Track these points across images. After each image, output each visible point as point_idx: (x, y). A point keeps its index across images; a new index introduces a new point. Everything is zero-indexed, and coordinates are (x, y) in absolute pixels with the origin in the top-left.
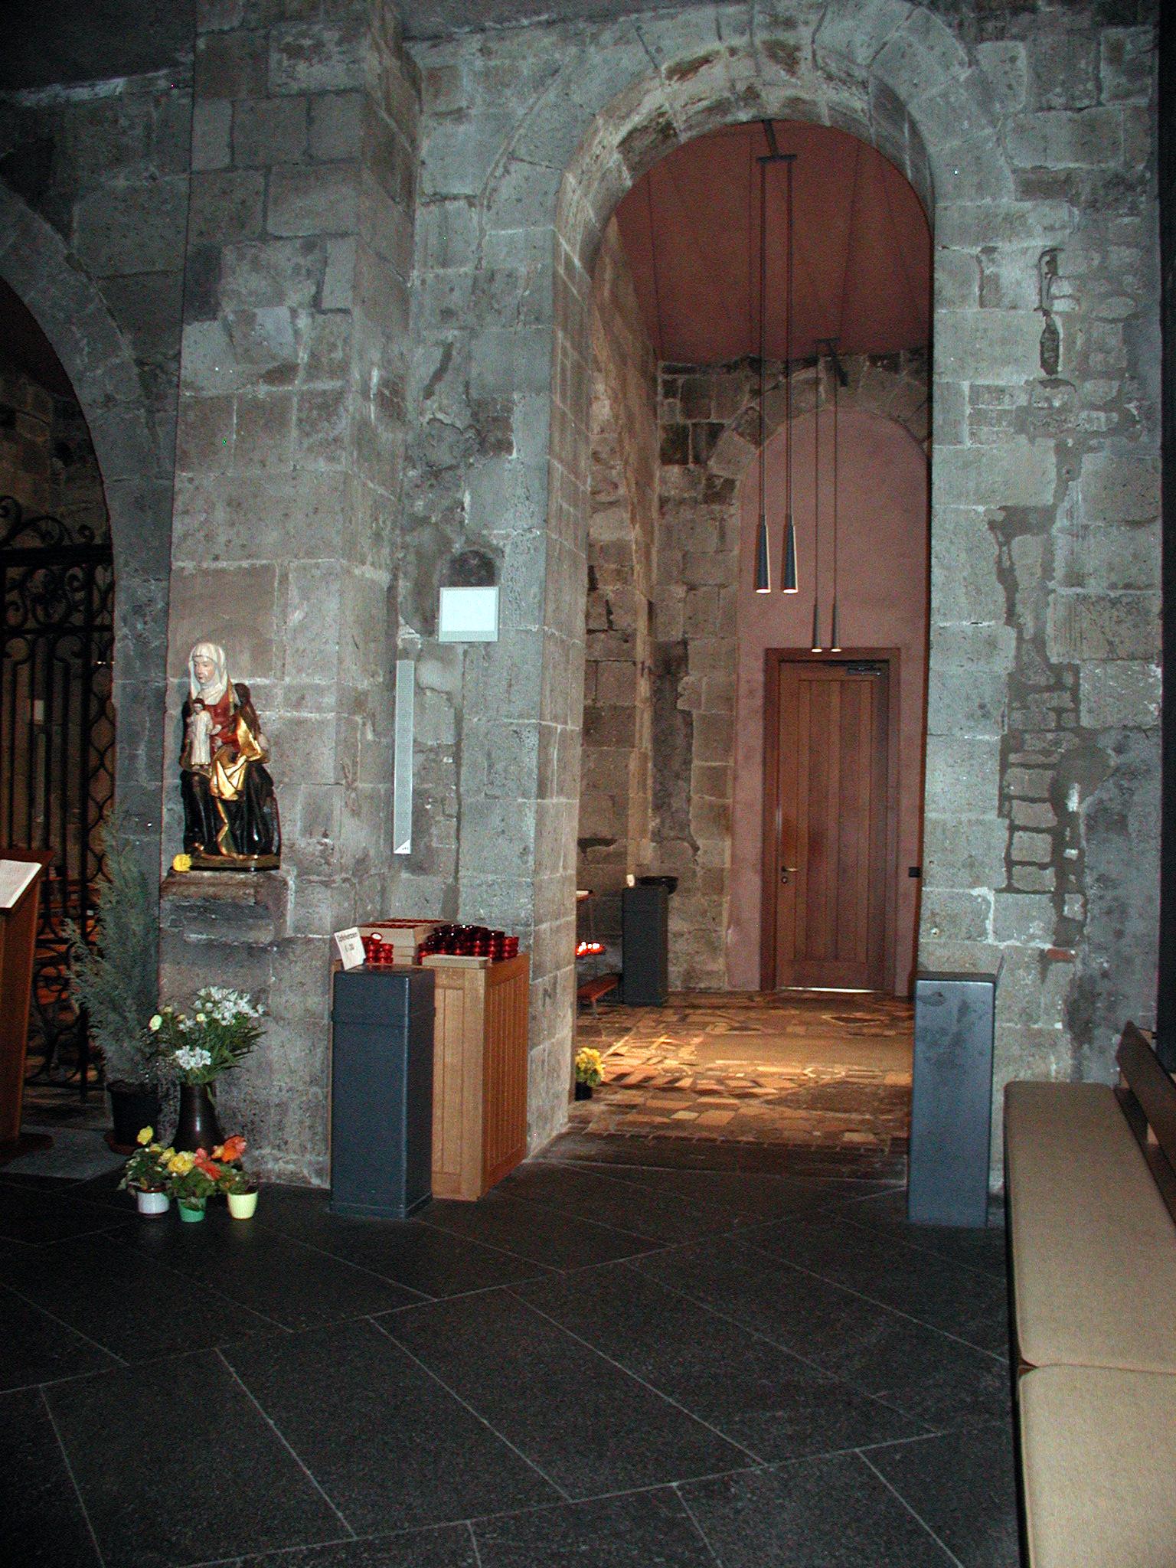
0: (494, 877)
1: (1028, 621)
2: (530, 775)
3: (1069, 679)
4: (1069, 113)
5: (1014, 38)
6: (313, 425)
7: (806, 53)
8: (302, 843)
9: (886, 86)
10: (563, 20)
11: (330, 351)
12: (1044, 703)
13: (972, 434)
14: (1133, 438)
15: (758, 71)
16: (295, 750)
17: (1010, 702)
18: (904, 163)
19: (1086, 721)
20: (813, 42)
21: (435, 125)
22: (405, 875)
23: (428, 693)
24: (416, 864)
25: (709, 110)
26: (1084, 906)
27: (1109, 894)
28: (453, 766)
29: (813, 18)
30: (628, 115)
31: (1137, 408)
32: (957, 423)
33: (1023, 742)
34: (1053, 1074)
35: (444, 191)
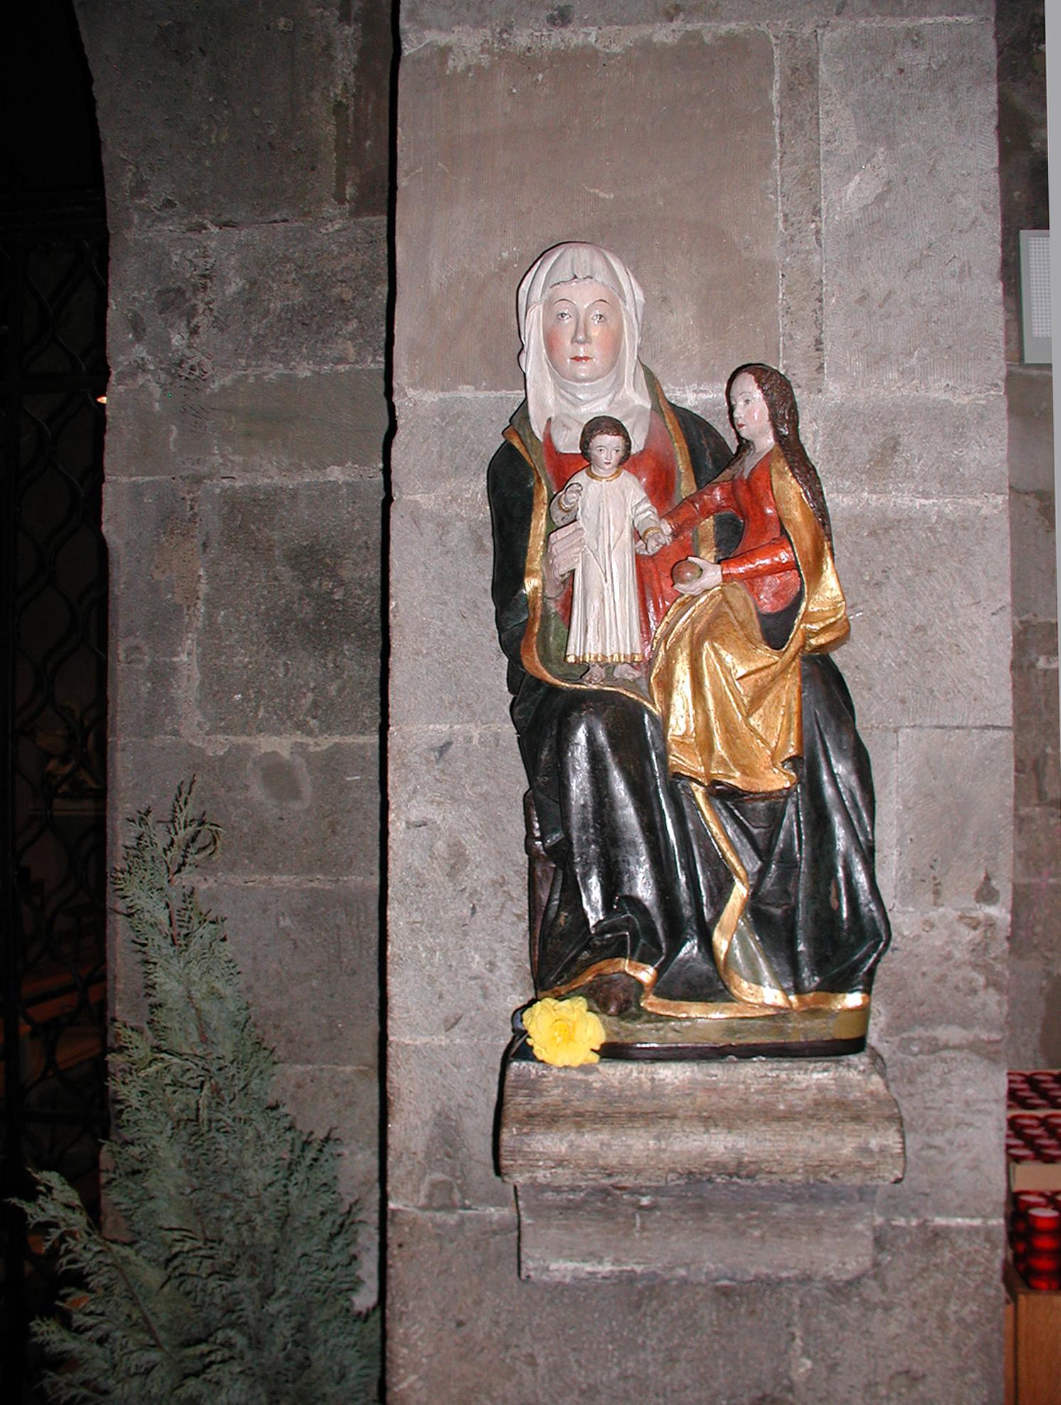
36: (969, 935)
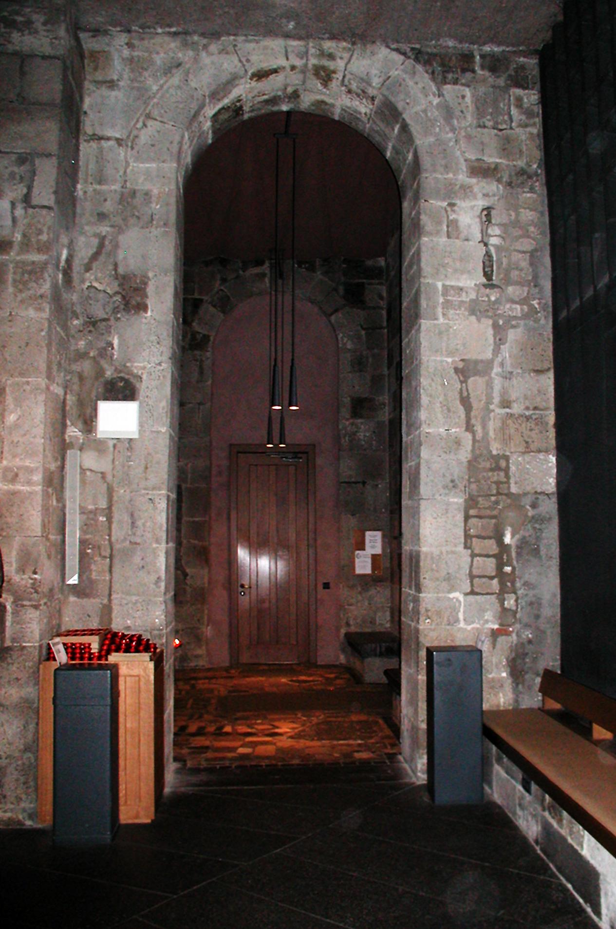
0: (138, 598)
1: (478, 429)
2: (161, 528)
3: (503, 464)
4: (496, 131)
5: (463, 85)
6: (25, 283)
7: (340, 76)
8: (16, 578)
9: (390, 102)
10: (186, 33)
11: (39, 234)
12: (489, 478)
13: (444, 315)
14: (537, 321)
15: (304, 82)
16: (10, 513)
17: (470, 478)
18: (387, 148)
19: (514, 489)
20: (345, 70)
21: (95, 89)
22: (72, 599)
23: (88, 473)
24: (78, 591)
25: (267, 102)
26: (516, 601)
27: (531, 593)
28: (106, 523)
29: (346, 55)
30: (223, 98)
31: (539, 304)
32: (435, 307)
33: (477, 503)
34: (502, 704)
35: (100, 133)
36: (31, 581)
